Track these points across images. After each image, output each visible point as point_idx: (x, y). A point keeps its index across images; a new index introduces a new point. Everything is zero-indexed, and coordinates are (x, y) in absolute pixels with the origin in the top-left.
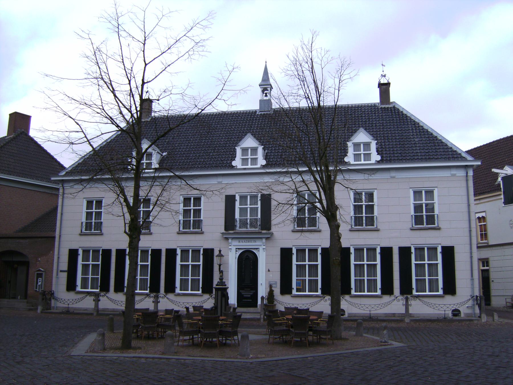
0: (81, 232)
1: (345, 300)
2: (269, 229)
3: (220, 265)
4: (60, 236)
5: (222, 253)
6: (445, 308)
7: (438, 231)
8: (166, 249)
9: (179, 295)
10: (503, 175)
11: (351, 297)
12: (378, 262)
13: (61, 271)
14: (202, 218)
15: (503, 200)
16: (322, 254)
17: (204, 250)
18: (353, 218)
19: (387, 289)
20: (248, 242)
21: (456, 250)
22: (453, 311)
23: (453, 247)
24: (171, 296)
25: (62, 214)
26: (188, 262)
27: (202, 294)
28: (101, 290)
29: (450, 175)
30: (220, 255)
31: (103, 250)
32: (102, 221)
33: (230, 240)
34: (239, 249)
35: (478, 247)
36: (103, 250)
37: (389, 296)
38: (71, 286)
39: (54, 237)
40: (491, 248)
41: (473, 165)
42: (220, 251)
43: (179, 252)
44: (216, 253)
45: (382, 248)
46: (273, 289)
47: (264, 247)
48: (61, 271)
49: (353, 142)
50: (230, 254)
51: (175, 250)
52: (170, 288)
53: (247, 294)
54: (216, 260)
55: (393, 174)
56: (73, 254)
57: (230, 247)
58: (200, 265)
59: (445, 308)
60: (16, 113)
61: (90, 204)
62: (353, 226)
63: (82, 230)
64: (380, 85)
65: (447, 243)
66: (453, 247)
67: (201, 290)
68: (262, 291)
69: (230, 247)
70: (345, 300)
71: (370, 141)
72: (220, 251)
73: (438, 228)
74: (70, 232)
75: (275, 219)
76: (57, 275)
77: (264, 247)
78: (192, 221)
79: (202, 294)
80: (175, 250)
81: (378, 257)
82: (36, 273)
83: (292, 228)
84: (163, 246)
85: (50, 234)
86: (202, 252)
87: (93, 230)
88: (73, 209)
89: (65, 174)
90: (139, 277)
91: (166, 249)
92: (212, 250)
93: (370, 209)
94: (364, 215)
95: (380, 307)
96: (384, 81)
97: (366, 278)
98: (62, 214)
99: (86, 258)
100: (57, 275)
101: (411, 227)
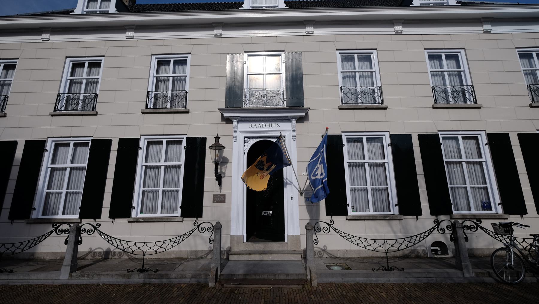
0: (147, 108)
3: (217, 164)
5: (221, 142)
8: (419, 135)
9: (137, 220)
11: (347, 219)
23: (508, 134)
24: (339, 221)
27: (181, 219)
28: (82, 217)
29: (482, 32)
30: (218, 146)
33: (235, 122)
34: (249, 138)
42: (217, 138)
44: (210, 142)
47: (295, 134)
50: (235, 145)
52: (122, 208)
54: (210, 156)
57: (235, 134)
63: (147, 106)
66: (508, 134)
69: (235, 134)
72: (217, 138)
77: (295, 134)
79: (181, 219)
80: (136, 141)
81: (388, 151)
84: (414, 129)
91: (419, 135)
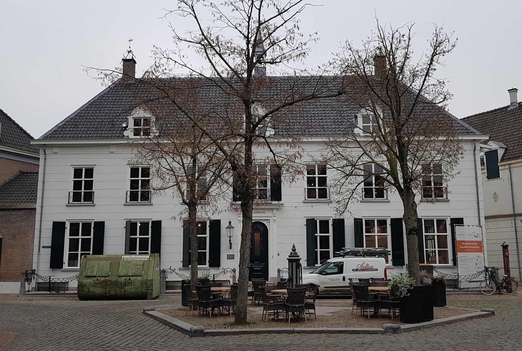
1: (176, 273)
2: (280, 199)
5: (232, 224)
7: (447, 203)
9: (67, 271)
10: (487, 150)
12: (331, 234)
13: (43, 247)
14: (93, 190)
15: (486, 174)
16: (391, 225)
17: (392, 220)
18: (306, 189)
21: (163, 224)
25: (44, 183)
31: (152, 221)
32: (93, 190)
33: (275, 211)
35: (486, 218)
36: (152, 221)
37: (400, 267)
38: (56, 263)
39: (35, 209)
40: (496, 219)
41: (481, 140)
43: (68, 225)
48: (43, 247)
49: (134, 116)
53: (257, 267)
55: (112, 149)
56: (58, 228)
58: (91, 239)
60: (135, 62)
61: (78, 173)
62: (307, 198)
64: (125, 61)
65: (155, 219)
67: (207, 263)
68: (277, 265)
70: (176, 273)
71: (150, 116)
73: (387, 201)
74: (54, 202)
75: (285, 189)
76: (39, 251)
78: (83, 193)
85: (31, 206)
86: (93, 226)
87: (82, 201)
88: (55, 179)
90: (319, 250)
92: (219, 221)
93: (89, 185)
94: (83, 190)
96: (129, 57)
98: (44, 183)
100: (39, 251)
101: (304, 200)
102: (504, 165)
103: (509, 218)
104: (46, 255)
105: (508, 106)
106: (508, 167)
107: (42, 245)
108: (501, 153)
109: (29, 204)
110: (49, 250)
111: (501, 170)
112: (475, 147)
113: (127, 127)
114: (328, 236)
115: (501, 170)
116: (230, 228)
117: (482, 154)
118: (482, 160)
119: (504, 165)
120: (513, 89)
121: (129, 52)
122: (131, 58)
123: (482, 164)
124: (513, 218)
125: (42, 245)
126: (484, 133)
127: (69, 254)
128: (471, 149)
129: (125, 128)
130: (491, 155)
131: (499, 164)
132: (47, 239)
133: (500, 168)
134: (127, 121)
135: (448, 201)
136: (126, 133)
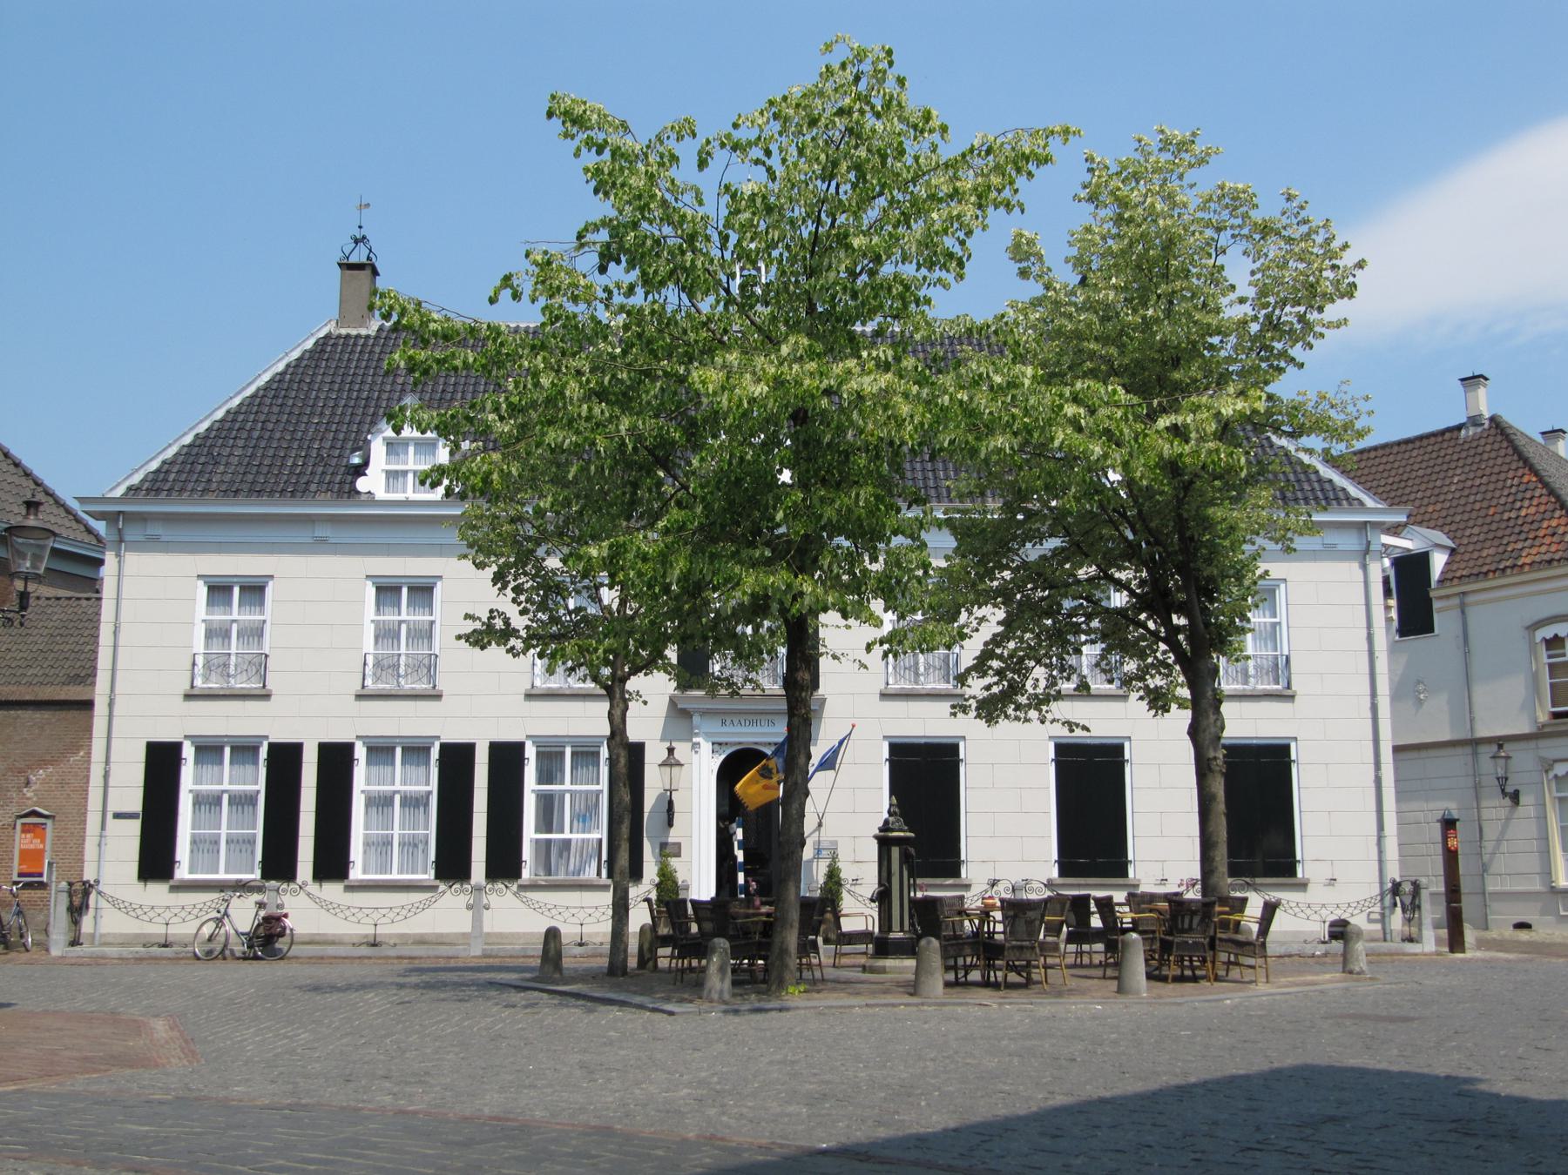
1: (308, 894)
4: (111, 705)
5: (677, 754)
6: (582, 915)
13: (117, 816)
19: (452, 865)
20: (752, 723)
22: (1333, 924)
26: (562, 783)
35: (1397, 749)
38: (156, 861)
39: (88, 705)
45: (444, 747)
46: (840, 865)
48: (117, 816)
51: (519, 748)
55: (322, 531)
56: (162, 762)
59: (582, 915)
70: (308, 894)
76: (103, 827)
80: (519, 748)
82: (19, 822)
83: (185, 686)
89: (126, 494)
95: (391, 915)
96: (359, 256)
97: (396, 832)
99: (548, 773)
100: (103, 827)
102: (1448, 597)
103: (1459, 750)
104: (127, 840)
105: (1459, 428)
106: (1456, 601)
107: (113, 807)
108: (1439, 561)
109: (79, 688)
110: (135, 826)
111: (1440, 610)
112: (1369, 543)
113: (366, 463)
114: (540, 782)
115: (1440, 610)
116: (671, 765)
117: (1387, 562)
118: (1386, 581)
119: (1448, 597)
120: (1474, 377)
121: (357, 241)
122: (364, 260)
123: (1387, 593)
124: (1468, 750)
125: (113, 807)
126: (1394, 501)
127: (193, 836)
128: (1357, 548)
129: (360, 470)
130: (1410, 570)
131: (1432, 594)
132: (129, 790)
133: (1436, 605)
134: (365, 448)
135: (1292, 698)
136: (362, 484)
